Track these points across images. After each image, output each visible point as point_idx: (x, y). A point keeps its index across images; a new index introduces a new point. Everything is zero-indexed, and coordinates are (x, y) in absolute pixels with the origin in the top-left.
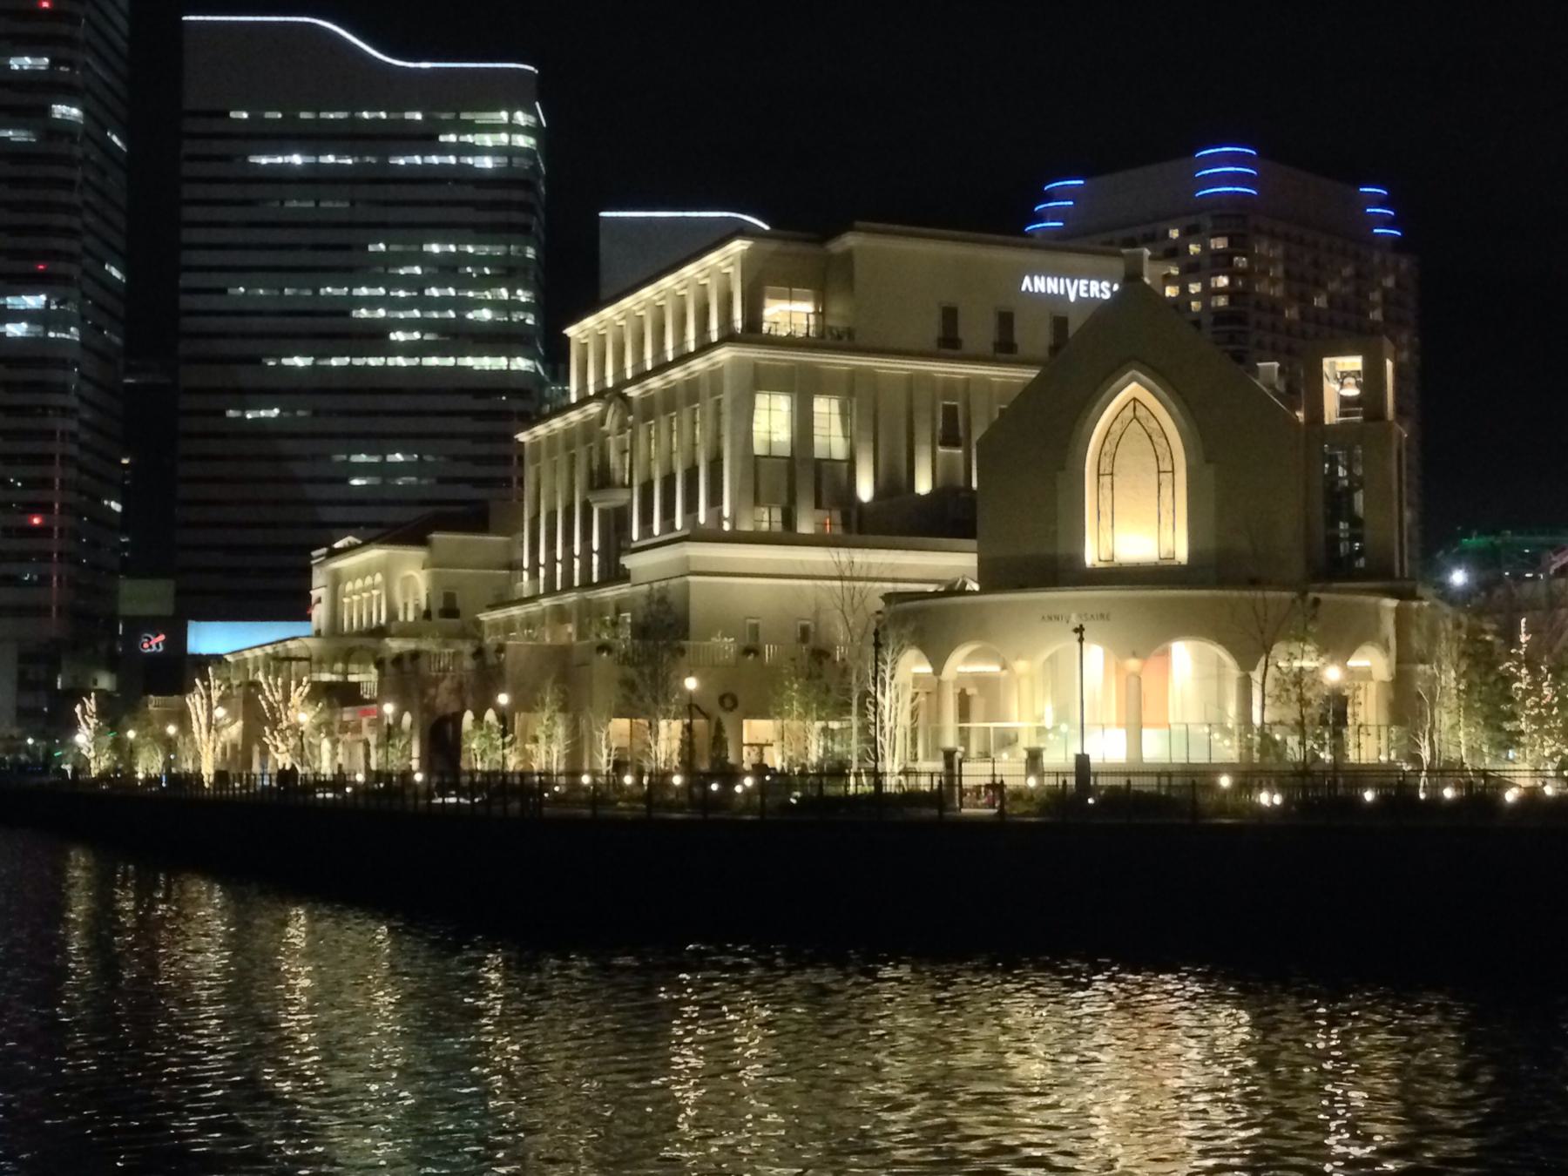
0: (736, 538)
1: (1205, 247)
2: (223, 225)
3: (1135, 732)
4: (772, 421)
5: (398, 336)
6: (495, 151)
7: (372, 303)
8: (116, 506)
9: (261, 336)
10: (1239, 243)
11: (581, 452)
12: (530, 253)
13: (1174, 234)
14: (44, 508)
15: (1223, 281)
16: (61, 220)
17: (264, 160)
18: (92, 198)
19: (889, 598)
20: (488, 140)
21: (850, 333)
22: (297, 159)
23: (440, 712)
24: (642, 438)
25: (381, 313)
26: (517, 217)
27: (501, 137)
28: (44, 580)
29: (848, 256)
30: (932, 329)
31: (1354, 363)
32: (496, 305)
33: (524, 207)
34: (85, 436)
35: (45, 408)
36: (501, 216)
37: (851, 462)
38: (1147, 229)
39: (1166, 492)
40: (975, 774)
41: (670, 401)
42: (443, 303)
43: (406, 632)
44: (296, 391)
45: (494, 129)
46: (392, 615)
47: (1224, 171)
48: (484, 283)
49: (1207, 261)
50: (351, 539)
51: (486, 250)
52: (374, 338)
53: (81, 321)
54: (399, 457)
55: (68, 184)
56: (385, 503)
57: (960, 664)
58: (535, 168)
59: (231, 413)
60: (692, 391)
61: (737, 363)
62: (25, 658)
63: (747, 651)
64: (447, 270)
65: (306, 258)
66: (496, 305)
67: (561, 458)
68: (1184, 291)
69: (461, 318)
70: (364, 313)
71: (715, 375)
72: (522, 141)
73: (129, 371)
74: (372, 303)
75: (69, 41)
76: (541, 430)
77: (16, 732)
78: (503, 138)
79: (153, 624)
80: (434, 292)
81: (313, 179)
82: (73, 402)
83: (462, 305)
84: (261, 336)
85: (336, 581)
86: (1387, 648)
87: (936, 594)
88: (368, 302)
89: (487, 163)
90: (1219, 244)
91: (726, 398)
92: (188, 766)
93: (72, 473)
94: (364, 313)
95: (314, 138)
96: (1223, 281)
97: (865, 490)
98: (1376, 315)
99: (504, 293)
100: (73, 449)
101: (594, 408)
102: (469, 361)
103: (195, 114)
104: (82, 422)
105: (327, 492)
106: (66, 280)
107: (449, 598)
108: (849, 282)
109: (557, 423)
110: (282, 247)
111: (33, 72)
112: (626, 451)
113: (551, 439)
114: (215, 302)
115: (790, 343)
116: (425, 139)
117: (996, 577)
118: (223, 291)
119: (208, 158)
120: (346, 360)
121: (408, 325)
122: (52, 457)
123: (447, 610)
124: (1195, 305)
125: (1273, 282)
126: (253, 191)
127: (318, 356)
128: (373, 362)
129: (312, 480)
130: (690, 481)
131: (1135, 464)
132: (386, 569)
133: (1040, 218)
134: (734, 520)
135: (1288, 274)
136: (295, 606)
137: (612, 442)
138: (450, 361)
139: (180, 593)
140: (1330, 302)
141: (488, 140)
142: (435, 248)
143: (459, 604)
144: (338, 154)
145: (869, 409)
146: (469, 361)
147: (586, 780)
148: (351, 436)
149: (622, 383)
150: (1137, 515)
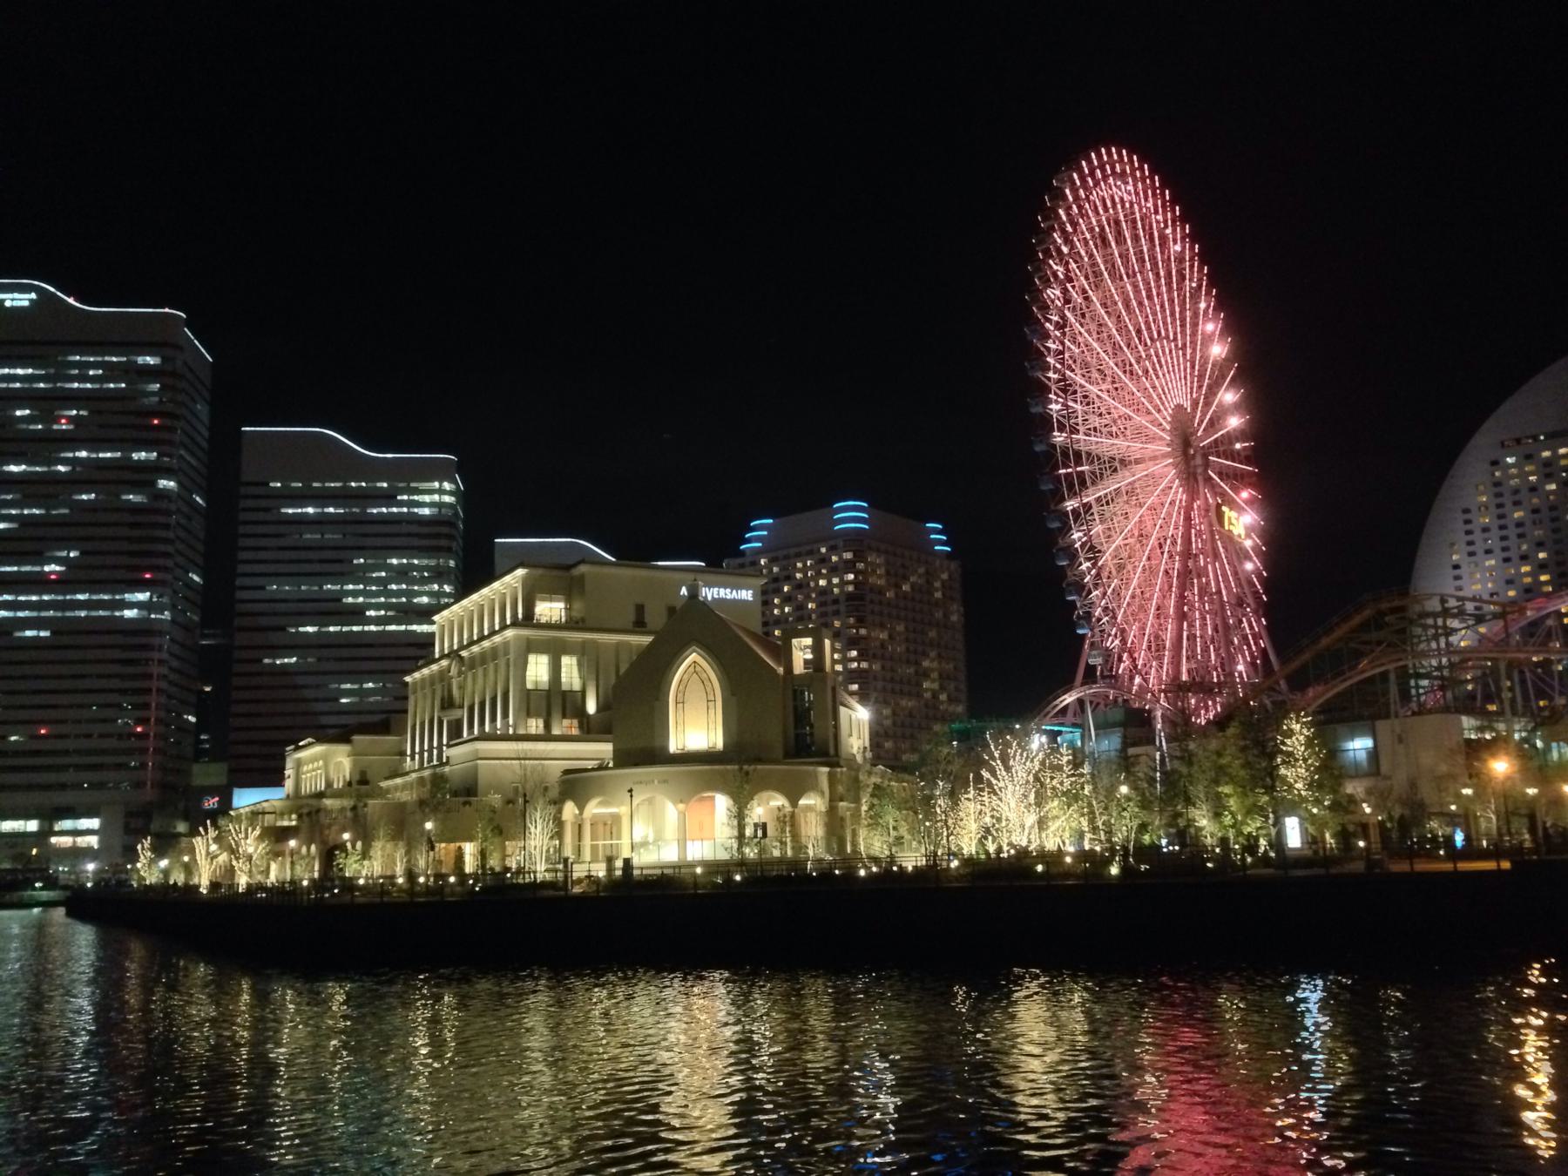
0: (505, 738)
1: (841, 558)
2: (265, 549)
3: (682, 843)
4: (538, 670)
5: (371, 613)
6: (431, 505)
7: (355, 594)
8: (192, 719)
9: (286, 614)
10: (859, 556)
11: (438, 687)
12: (452, 563)
13: (823, 550)
14: (142, 721)
15: (851, 577)
16: (162, 548)
17: (290, 511)
18: (182, 534)
19: (567, 772)
20: (427, 498)
21: (583, 620)
22: (310, 510)
23: (331, 844)
24: (469, 680)
25: (361, 599)
26: (443, 542)
27: (436, 496)
28: (143, 766)
29: (582, 577)
30: (632, 617)
31: (808, 641)
32: (430, 594)
33: (450, 537)
34: (172, 676)
35: (147, 660)
36: (434, 542)
37: (583, 692)
38: (808, 548)
39: (712, 711)
40: (579, 871)
41: (483, 658)
42: (399, 594)
43: (338, 794)
44: (309, 647)
45: (431, 492)
46: (329, 784)
47: (850, 514)
48: (423, 581)
49: (841, 566)
50: (310, 740)
51: (425, 562)
52: (357, 614)
53: (173, 608)
54: (371, 685)
55: (167, 527)
56: (359, 713)
57: (594, 808)
58: (456, 514)
59: (266, 661)
60: (494, 653)
61: (517, 638)
62: (130, 814)
63: (509, 802)
64: (402, 574)
65: (317, 568)
66: (430, 594)
67: (428, 691)
68: (829, 582)
69: (409, 602)
70: (350, 600)
71: (506, 644)
72: (447, 499)
73: (205, 637)
74: (355, 594)
75: (171, 443)
76: (417, 675)
77: (120, 861)
78: (436, 497)
79: (211, 791)
80: (394, 587)
81: (320, 522)
82: (165, 656)
83: (410, 594)
84: (286, 614)
85: (299, 764)
86: (823, 793)
87: (593, 769)
88: (353, 593)
89: (426, 511)
90: (848, 556)
91: (512, 657)
92: (196, 881)
93: (163, 700)
94: (350, 600)
95: (321, 498)
96: (851, 577)
97: (591, 707)
98: (938, 595)
99: (436, 587)
100: (164, 685)
101: (444, 663)
102: (414, 627)
103: (248, 484)
104: (170, 668)
105: (325, 707)
106: (163, 583)
107: (363, 773)
108: (582, 592)
109: (425, 671)
110: (299, 561)
111: (147, 461)
112: (462, 687)
113: (423, 680)
114: (258, 595)
115: (549, 626)
116: (389, 498)
117: (625, 759)
118: (263, 588)
119: (258, 510)
120: (338, 628)
121: (378, 607)
122: (150, 690)
123: (362, 782)
124: (836, 590)
125: (880, 577)
126: (282, 529)
127: (321, 625)
128: (355, 628)
129: (317, 700)
130: (492, 704)
131: (695, 693)
132: (325, 758)
133: (749, 541)
134: (515, 727)
135: (888, 573)
136: (276, 779)
137: (455, 683)
138: (403, 628)
139: (231, 771)
140: (912, 587)
141: (427, 498)
142: (395, 561)
143: (369, 776)
144: (336, 507)
145: (590, 660)
146: (414, 627)
147: (422, 880)
148: (340, 673)
149: (462, 647)
150: (696, 726)
